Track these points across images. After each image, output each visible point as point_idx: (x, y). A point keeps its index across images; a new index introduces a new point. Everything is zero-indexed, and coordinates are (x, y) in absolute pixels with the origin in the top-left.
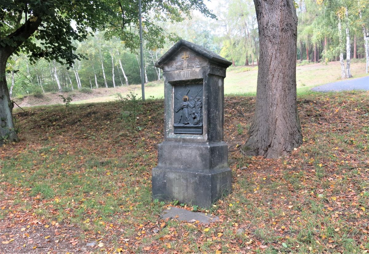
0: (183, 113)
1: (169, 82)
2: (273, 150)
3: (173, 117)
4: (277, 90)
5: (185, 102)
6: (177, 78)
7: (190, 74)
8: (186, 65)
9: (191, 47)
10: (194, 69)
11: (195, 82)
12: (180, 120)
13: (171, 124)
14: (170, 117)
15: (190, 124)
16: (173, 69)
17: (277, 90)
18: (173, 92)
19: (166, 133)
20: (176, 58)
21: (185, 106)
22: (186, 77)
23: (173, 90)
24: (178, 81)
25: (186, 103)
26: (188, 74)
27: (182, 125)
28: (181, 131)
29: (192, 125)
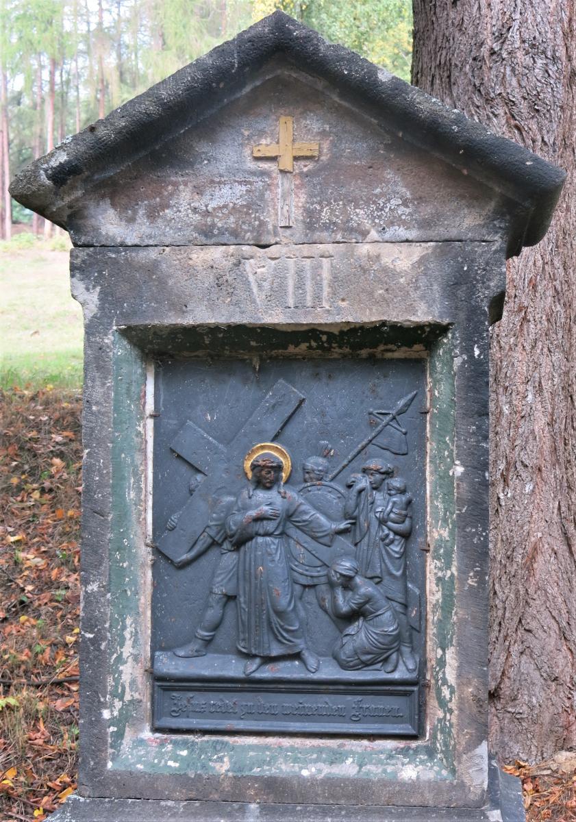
0: (244, 574)
1: (129, 333)
2: (517, 718)
3: (145, 600)
4: (539, 390)
5: (261, 495)
6: (212, 306)
7: (335, 278)
8: (297, 214)
9: (376, 83)
10: (364, 249)
11: (356, 347)
12: (216, 627)
13: (136, 658)
14: (126, 606)
15: (312, 661)
16: (170, 235)
17: (539, 390)
18: (150, 407)
19: (101, 738)
20: (203, 147)
21: (270, 526)
22: (291, 302)
23: (150, 388)
24: (214, 330)
25: (273, 495)
26: (318, 285)
27: (234, 668)
28: (226, 714)
29: (329, 672)
